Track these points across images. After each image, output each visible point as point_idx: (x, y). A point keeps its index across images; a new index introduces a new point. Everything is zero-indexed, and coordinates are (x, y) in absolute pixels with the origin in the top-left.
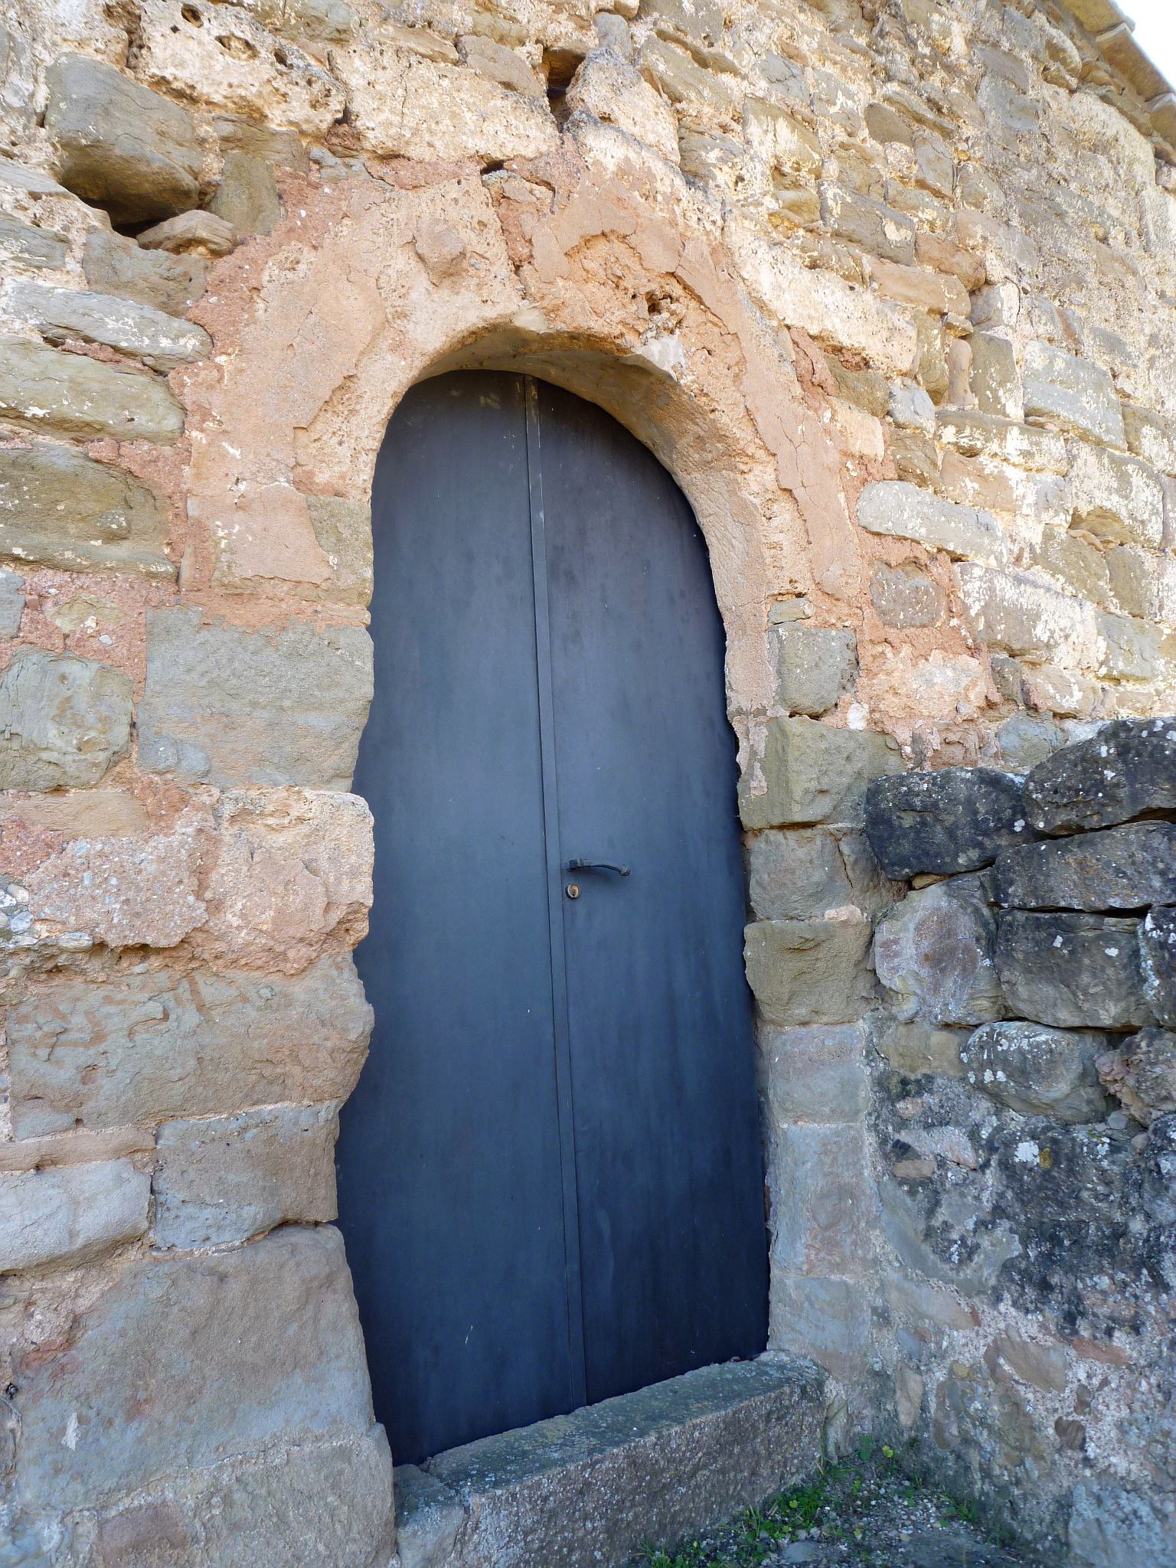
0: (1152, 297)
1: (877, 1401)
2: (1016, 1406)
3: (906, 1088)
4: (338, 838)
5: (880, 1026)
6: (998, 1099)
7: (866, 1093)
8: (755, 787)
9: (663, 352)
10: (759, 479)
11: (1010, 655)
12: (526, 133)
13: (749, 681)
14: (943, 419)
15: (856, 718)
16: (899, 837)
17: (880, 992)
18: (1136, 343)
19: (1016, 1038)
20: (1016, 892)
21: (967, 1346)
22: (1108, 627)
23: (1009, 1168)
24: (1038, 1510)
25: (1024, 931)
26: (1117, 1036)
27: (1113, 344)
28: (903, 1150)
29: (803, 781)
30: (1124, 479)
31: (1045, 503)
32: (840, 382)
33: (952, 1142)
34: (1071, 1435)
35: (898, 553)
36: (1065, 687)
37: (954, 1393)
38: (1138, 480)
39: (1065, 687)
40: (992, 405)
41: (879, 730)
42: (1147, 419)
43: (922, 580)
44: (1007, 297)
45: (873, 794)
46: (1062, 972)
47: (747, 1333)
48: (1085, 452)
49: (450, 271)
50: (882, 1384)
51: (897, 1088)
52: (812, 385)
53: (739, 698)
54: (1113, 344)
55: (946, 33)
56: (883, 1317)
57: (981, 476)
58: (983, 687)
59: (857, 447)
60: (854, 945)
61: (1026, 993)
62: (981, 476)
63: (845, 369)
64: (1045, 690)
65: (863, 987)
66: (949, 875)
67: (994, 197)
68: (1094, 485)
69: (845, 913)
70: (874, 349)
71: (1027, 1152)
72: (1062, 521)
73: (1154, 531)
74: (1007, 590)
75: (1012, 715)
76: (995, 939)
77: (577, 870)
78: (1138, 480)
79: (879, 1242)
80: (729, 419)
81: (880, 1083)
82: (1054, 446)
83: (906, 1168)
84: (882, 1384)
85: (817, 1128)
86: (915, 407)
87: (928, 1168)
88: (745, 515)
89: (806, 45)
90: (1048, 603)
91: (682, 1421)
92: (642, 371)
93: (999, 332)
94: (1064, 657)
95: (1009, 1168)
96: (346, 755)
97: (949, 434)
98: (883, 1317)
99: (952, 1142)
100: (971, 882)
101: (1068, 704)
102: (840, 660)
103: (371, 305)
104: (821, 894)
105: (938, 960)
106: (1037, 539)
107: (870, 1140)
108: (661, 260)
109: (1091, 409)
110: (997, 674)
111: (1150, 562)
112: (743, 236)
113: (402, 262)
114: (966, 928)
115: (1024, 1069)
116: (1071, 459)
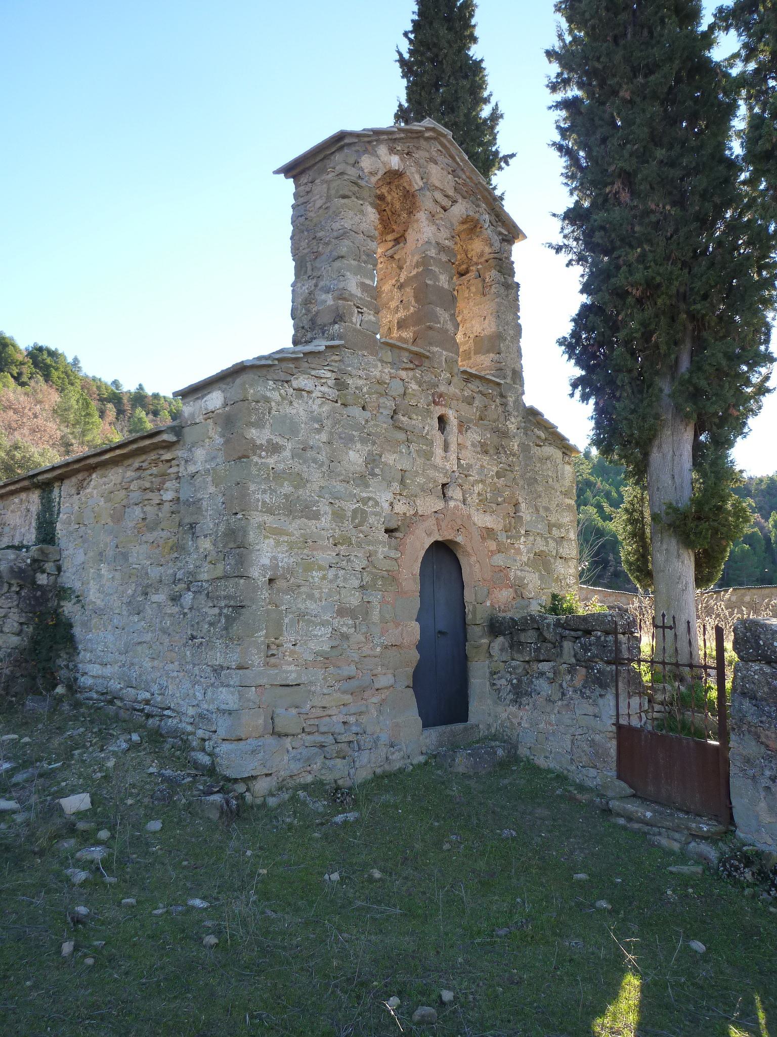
0: (558, 493)
1: (488, 730)
2: (512, 722)
3: (495, 673)
4: (415, 627)
5: (490, 662)
6: (511, 673)
7: (488, 674)
8: (469, 617)
9: (459, 539)
10: (473, 559)
11: (519, 588)
12: (440, 505)
13: (468, 596)
14: (508, 538)
15: (488, 604)
16: (495, 627)
17: (491, 656)
18: (553, 506)
19: (514, 663)
20: (515, 639)
21: (504, 716)
22: (541, 578)
23: (512, 684)
24: (514, 738)
25: (516, 645)
26: (528, 662)
27: (547, 509)
28: (494, 684)
29: (479, 617)
30: (547, 542)
31: (528, 552)
32: (488, 535)
33: (503, 682)
34: (519, 724)
35: (497, 569)
36: (530, 592)
37: (502, 725)
38: (551, 541)
39: (530, 592)
40: (519, 532)
41: (492, 605)
42: (554, 526)
43: (502, 574)
44: (523, 506)
45: (491, 619)
46: (519, 651)
47: (464, 718)
48: (538, 539)
49: (429, 535)
50: (489, 726)
51: (493, 673)
52: (483, 538)
53: (466, 599)
54: (547, 509)
55: (513, 446)
56: (489, 715)
57: (515, 549)
58: (513, 595)
59: (491, 549)
60: (486, 647)
61: (516, 656)
62: (515, 549)
63: (489, 533)
64: (527, 594)
65: (487, 655)
66: (504, 635)
67: (521, 483)
68: (540, 545)
69: (485, 641)
70: (495, 527)
71: (515, 681)
72: (532, 555)
73: (554, 553)
74: (519, 573)
75: (519, 599)
76: (511, 647)
77: (440, 632)
78: (551, 541)
79: (489, 702)
80: (469, 549)
81: (491, 673)
82: (531, 538)
83: (495, 687)
84: (489, 726)
85: (478, 681)
86: (502, 537)
87: (498, 687)
88: (470, 565)
89: (485, 464)
90: (527, 574)
91: (459, 727)
92: (456, 543)
93: (521, 514)
94: (531, 586)
95: (512, 684)
96: (415, 617)
97: (509, 541)
98: (489, 715)
99: (503, 682)
100: (508, 637)
101: (531, 596)
102: (486, 593)
103: (420, 541)
104: (481, 637)
105: (502, 650)
106: (526, 560)
107: (488, 683)
108: (459, 522)
109: (541, 527)
110: (516, 592)
111: (552, 561)
112: (473, 511)
113: (424, 534)
114: (507, 645)
115: (514, 668)
116: (535, 540)
